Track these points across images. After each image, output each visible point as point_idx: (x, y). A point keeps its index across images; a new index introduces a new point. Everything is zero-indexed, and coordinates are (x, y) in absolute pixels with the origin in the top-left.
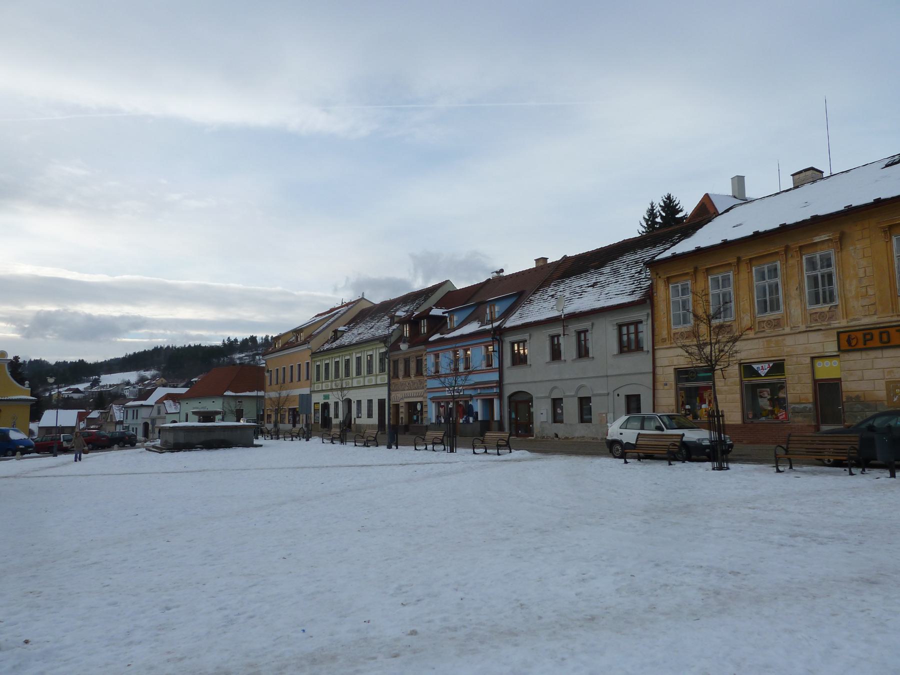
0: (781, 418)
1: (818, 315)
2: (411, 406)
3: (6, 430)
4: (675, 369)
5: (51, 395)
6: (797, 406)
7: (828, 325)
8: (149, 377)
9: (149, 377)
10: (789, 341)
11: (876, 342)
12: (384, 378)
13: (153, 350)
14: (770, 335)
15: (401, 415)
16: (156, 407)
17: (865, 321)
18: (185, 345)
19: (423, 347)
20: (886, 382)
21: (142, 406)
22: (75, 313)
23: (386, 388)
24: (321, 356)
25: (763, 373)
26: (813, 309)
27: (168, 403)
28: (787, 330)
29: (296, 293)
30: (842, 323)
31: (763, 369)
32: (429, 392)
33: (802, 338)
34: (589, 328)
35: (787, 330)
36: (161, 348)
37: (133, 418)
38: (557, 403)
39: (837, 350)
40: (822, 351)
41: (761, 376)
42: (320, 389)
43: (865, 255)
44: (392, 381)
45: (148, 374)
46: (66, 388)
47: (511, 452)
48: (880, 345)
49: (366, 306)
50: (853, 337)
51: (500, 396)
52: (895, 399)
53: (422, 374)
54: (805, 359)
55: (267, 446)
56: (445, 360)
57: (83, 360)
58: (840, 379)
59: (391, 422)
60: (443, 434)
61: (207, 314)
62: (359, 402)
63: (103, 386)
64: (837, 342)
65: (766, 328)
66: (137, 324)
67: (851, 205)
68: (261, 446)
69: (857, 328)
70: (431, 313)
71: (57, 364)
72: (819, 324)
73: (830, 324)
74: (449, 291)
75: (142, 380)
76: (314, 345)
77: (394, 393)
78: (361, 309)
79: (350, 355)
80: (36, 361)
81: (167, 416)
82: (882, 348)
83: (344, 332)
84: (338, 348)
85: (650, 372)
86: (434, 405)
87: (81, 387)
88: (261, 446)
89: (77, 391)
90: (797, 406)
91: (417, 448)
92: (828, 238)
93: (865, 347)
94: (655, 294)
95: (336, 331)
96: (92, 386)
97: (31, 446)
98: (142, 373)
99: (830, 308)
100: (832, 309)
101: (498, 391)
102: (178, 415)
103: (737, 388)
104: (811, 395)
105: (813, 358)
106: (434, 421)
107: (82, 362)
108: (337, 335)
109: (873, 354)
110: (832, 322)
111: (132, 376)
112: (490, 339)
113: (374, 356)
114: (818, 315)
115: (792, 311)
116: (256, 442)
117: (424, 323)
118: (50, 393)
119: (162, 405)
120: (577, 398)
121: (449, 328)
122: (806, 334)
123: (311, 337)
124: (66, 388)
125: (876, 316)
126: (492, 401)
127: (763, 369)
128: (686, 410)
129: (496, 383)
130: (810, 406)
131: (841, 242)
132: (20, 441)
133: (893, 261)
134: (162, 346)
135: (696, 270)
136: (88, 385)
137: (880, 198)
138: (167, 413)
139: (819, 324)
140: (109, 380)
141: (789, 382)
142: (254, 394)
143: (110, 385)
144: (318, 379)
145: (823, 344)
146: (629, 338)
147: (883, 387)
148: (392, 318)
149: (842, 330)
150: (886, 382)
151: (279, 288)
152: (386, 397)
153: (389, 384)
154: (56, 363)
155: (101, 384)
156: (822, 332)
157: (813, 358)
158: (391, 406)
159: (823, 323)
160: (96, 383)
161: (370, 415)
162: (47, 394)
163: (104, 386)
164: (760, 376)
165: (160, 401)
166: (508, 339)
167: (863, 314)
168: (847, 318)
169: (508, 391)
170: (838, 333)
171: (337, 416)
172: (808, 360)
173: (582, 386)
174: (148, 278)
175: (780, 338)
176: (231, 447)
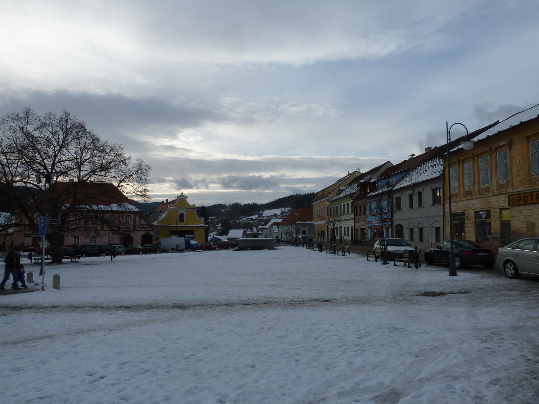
0: (490, 241)
1: (502, 185)
2: (363, 230)
3: (189, 240)
4: (474, 211)
5: (240, 222)
6: (495, 235)
7: (506, 191)
8: (287, 211)
9: (287, 211)
10: (492, 199)
11: (522, 202)
12: (352, 216)
13: (289, 197)
14: (485, 196)
15: (359, 235)
16: (269, 229)
17: (520, 189)
18: (306, 194)
19: (364, 200)
20: (527, 223)
21: (264, 228)
22: (248, 176)
23: (353, 221)
24: (335, 202)
25: (484, 216)
26: (501, 182)
27: (274, 227)
28: (491, 194)
29: (362, 158)
30: (510, 190)
31: (483, 214)
32: (368, 223)
33: (496, 198)
34: (422, 190)
35: (491, 194)
36: (293, 195)
37: (421, 230)
38: (412, 230)
39: (508, 205)
40: (503, 205)
41: (483, 219)
42: (349, 218)
43: (520, 153)
44: (356, 217)
45: (286, 210)
46: (247, 218)
47: (350, 254)
48: (524, 203)
49: (358, 175)
50: (514, 198)
51: (392, 226)
52: (530, 233)
53: (365, 214)
54: (498, 209)
55: (279, 249)
56: (374, 205)
57: (255, 203)
58: (509, 221)
59: (356, 239)
60: (349, 246)
61: (314, 175)
62: (345, 228)
63: (263, 217)
64: (508, 201)
65: (484, 192)
66: (281, 180)
67: (512, 125)
68: (276, 249)
69: (516, 193)
70: (370, 181)
71: (245, 205)
72: (502, 191)
73: (506, 191)
74: (389, 167)
75: (283, 213)
76: (330, 197)
77: (356, 223)
78: (355, 177)
79: (341, 203)
80: (235, 204)
81: (274, 233)
82: (525, 205)
83: (343, 190)
84: (345, 197)
85: (442, 215)
86: (370, 230)
87: (254, 217)
88: (276, 249)
89: (252, 219)
90: (495, 235)
91: (339, 254)
92: (504, 143)
93: (537, 202)
94: (445, 173)
95: (339, 190)
96: (259, 216)
97: (198, 247)
98: (284, 209)
99: (507, 182)
100: (508, 183)
101: (391, 224)
102: (278, 233)
103: (473, 225)
104: (499, 229)
105: (501, 210)
106: (370, 239)
107: (254, 204)
108: (340, 191)
109: (523, 208)
110: (508, 190)
111: (278, 211)
112: (387, 196)
113: (349, 203)
114: (502, 185)
115: (493, 183)
116: (274, 247)
117: (368, 186)
118: (240, 220)
119: (272, 228)
120: (418, 228)
121: (391, 185)
122: (497, 196)
123: (329, 193)
124: (247, 218)
125: (523, 187)
126: (388, 228)
127: (483, 214)
128: (457, 236)
129: (389, 219)
130: (499, 235)
131: (510, 144)
132: (194, 244)
133: (529, 156)
134: (294, 194)
135: (459, 161)
136: (257, 216)
137: (522, 122)
138: (274, 232)
139: (502, 191)
140: (267, 213)
141: (492, 222)
142: (309, 222)
143: (267, 216)
144: (344, 213)
145: (504, 202)
146: (437, 195)
147: (525, 226)
148: (358, 183)
149: (511, 194)
150: (527, 223)
151: (351, 157)
152: (353, 225)
153: (354, 219)
154: (245, 204)
155: (263, 216)
156: (504, 195)
157: (501, 210)
158: (355, 230)
159: (504, 190)
160: (261, 215)
161: (348, 235)
162: (238, 221)
163: (264, 216)
164: (482, 218)
165: (271, 226)
166: (395, 196)
167: (519, 185)
168: (513, 188)
169: (396, 223)
170: (509, 196)
171: (337, 235)
172: (498, 210)
173: (419, 222)
174: (282, 156)
175: (489, 198)
176: (263, 249)
